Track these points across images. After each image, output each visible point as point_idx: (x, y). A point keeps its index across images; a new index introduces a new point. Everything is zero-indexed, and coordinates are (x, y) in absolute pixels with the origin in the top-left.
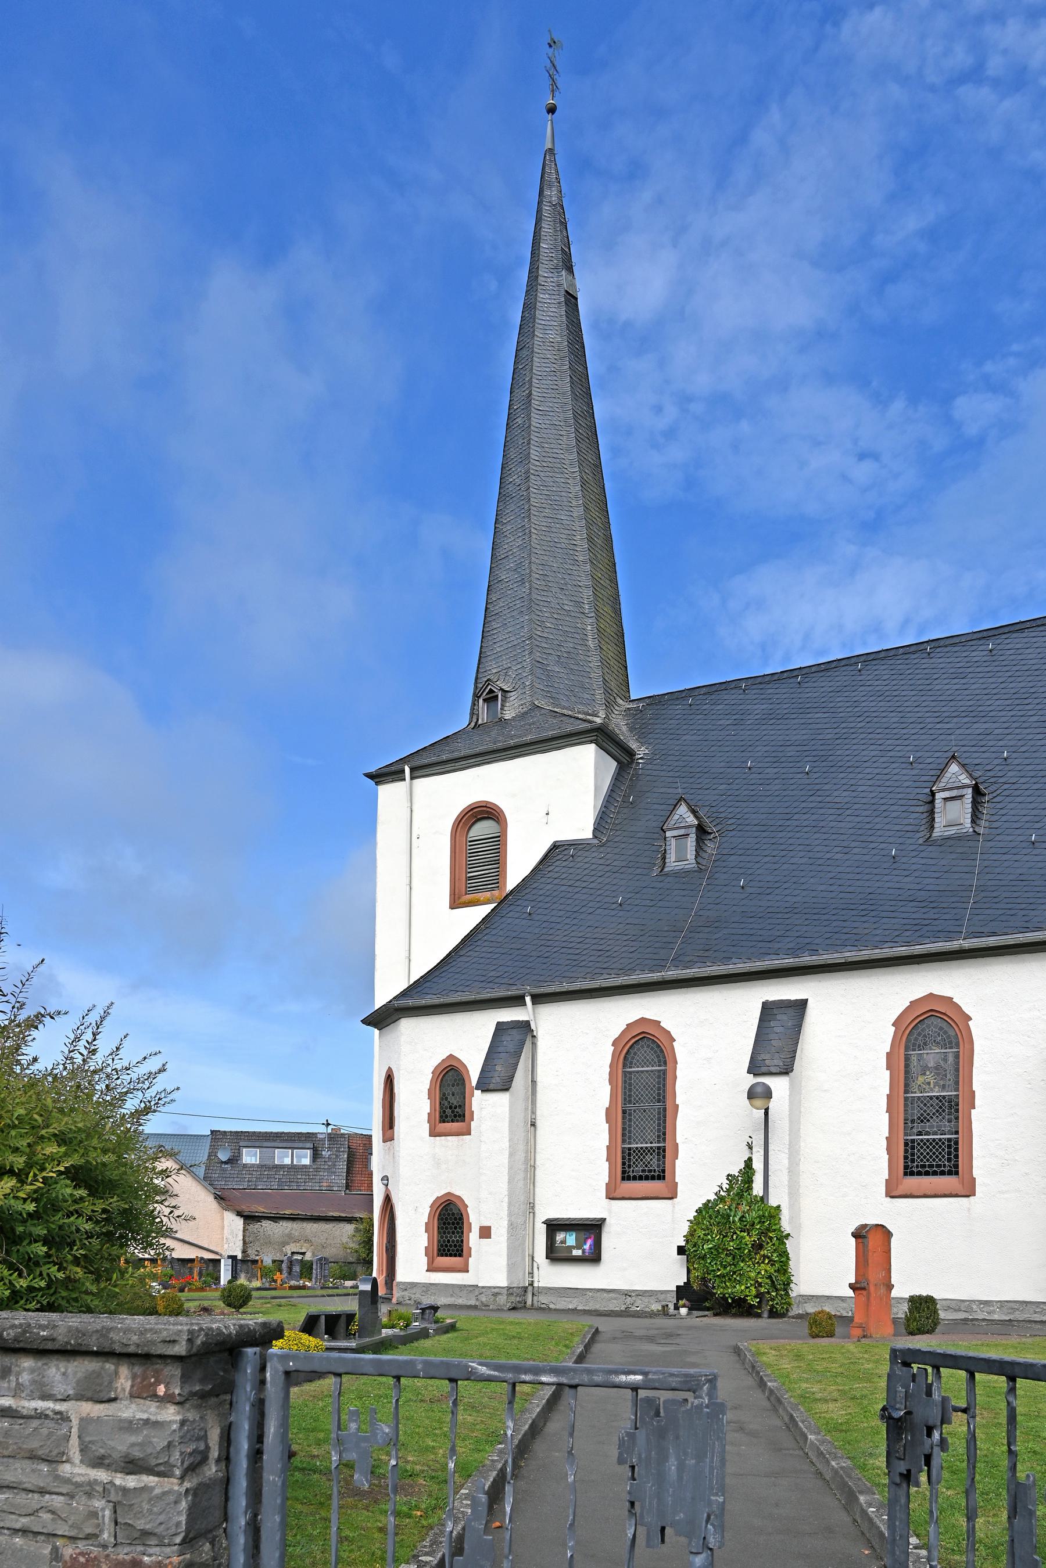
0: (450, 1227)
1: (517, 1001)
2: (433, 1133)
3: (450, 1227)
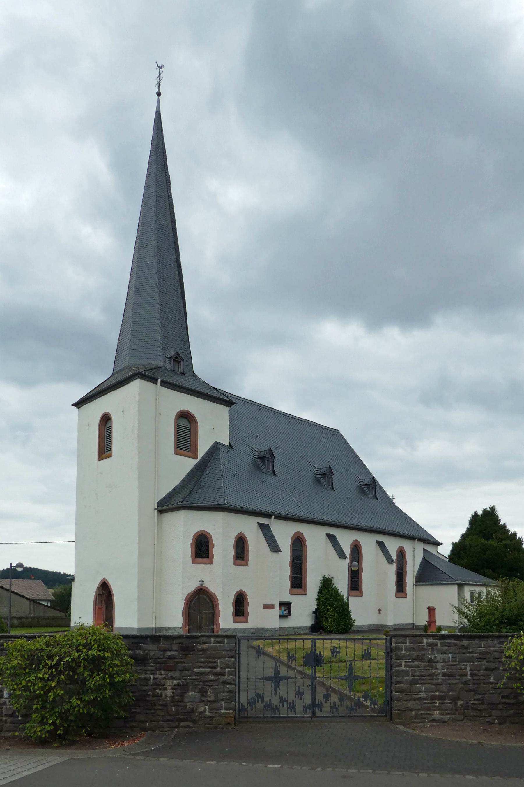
0: (240, 603)
1: (268, 515)
3: (240, 603)
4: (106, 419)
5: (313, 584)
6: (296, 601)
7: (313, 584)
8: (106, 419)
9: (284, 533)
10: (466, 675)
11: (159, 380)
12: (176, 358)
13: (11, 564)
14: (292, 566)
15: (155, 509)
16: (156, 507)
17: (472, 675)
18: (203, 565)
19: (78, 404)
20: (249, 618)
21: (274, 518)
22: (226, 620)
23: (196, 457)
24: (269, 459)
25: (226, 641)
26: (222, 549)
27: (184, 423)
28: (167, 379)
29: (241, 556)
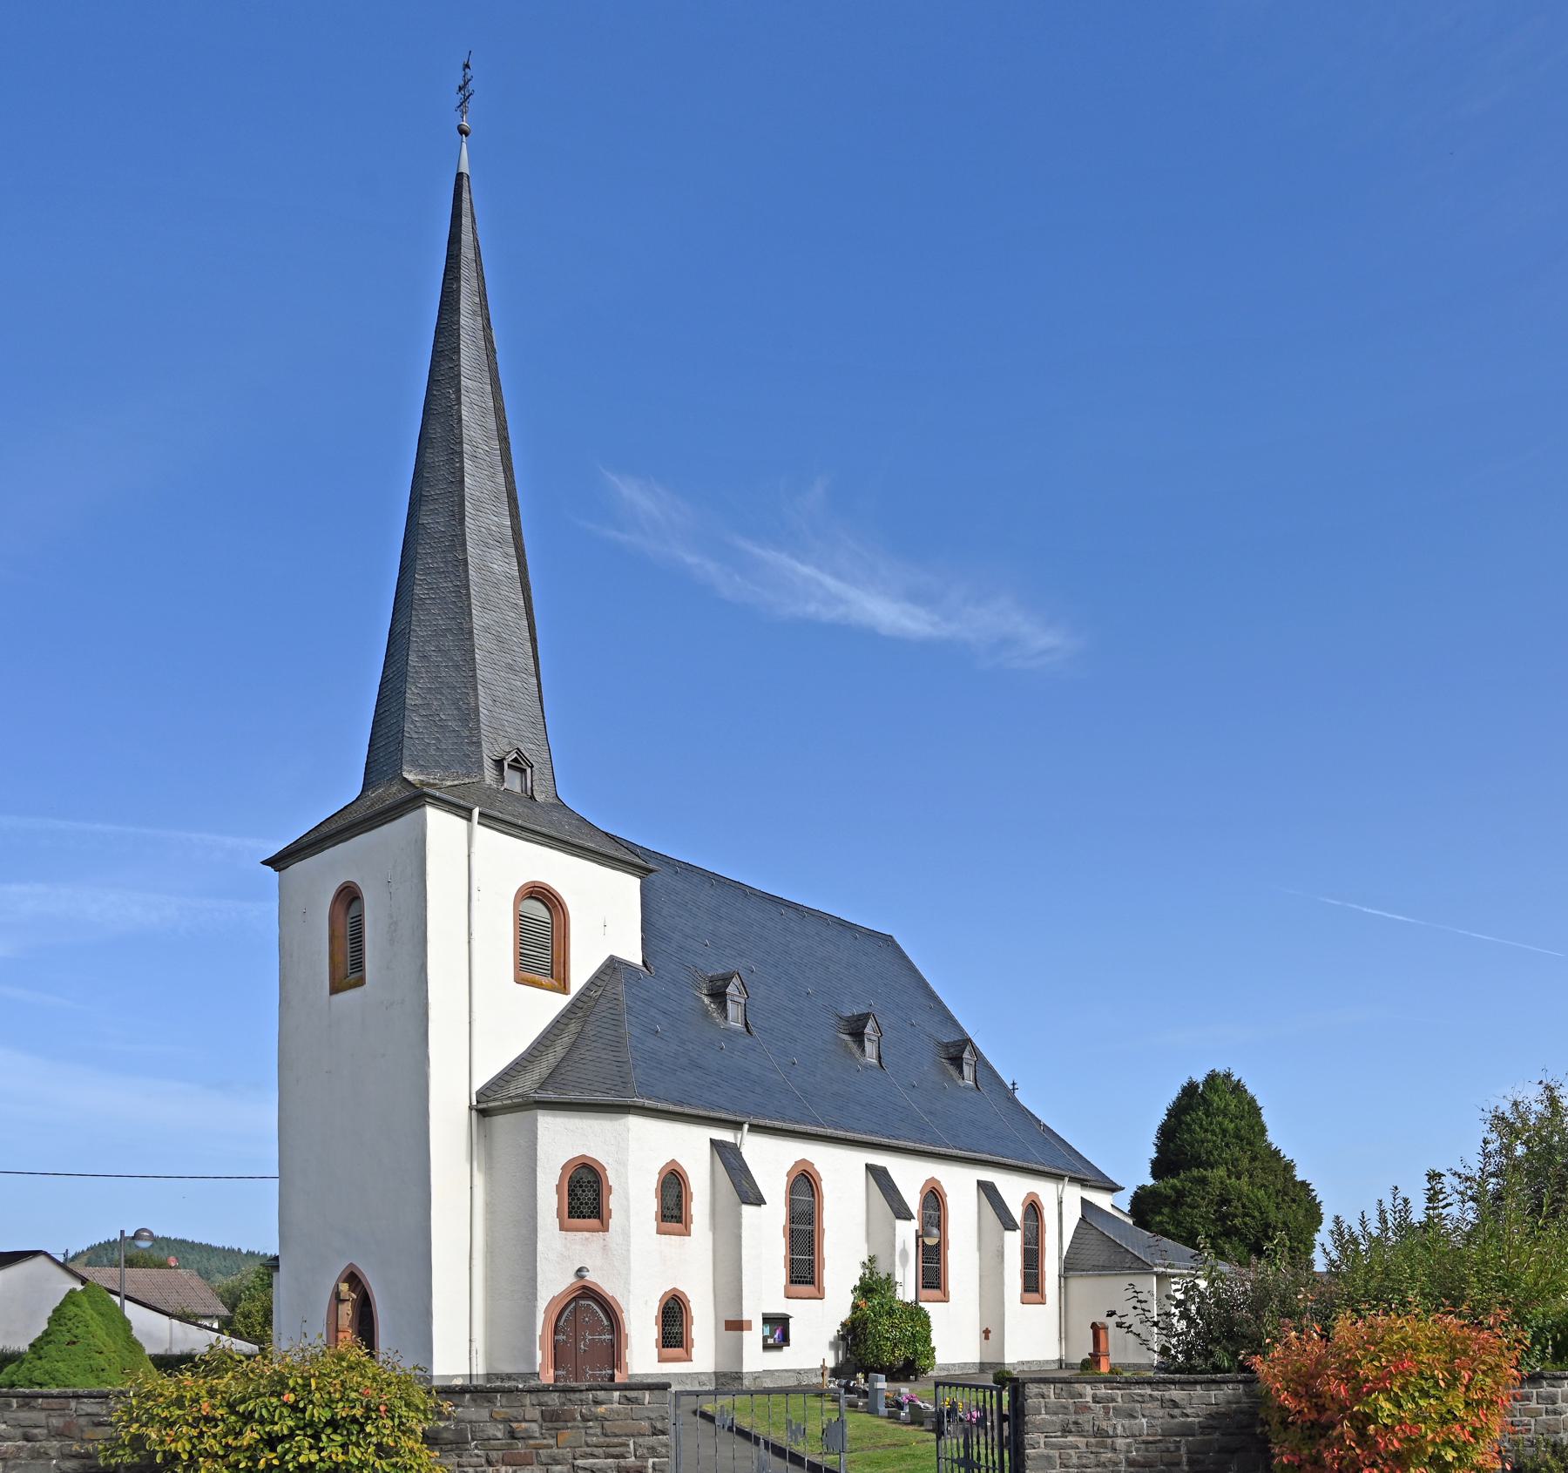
0: (673, 1315)
1: (736, 1126)
2: (659, 1232)
3: (673, 1315)
4: (349, 896)
5: (841, 1269)
6: (801, 1313)
7: (841, 1269)
8: (349, 896)
9: (772, 1161)
10: (1178, 1464)
11: (476, 811)
12: (515, 760)
13: (122, 1232)
14: (791, 1236)
15: (471, 1108)
17: (1190, 1462)
18: (587, 1234)
19: (278, 862)
20: (695, 1352)
22: (642, 1355)
23: (564, 989)
25: (647, 1395)
26: (633, 1198)
27: (538, 910)
28: (755, 1122)
29: (675, 1212)
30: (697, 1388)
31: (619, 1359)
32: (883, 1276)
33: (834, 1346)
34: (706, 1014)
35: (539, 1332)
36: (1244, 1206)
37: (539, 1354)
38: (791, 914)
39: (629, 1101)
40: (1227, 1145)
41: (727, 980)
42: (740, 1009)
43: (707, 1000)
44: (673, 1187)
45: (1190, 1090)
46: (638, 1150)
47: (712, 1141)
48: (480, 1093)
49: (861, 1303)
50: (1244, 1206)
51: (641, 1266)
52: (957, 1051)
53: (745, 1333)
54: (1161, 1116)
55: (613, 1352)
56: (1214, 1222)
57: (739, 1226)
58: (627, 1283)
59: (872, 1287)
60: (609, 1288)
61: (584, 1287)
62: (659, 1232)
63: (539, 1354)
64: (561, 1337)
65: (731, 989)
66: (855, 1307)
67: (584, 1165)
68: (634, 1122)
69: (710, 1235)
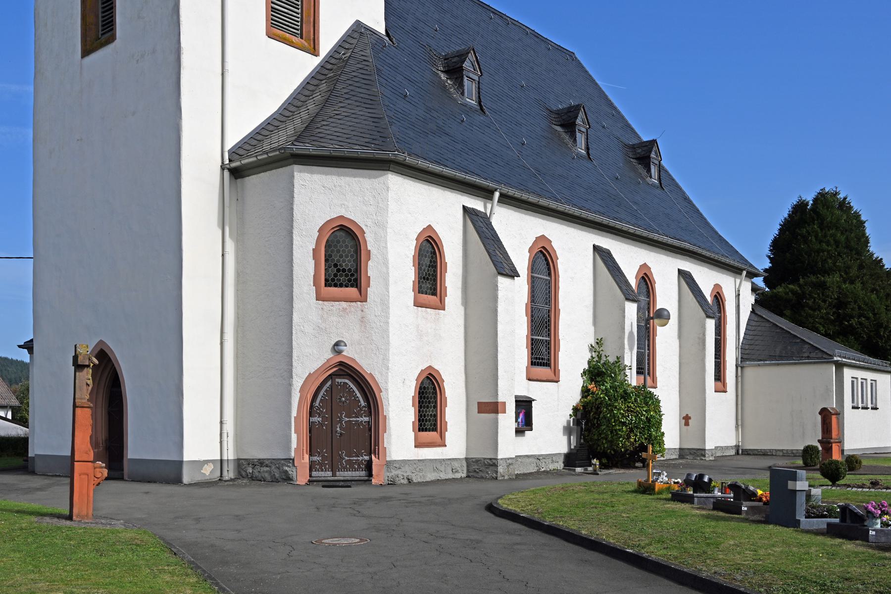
0: (429, 393)
1: (486, 193)
2: (417, 304)
3: (429, 393)
9: (517, 231)
15: (223, 168)
16: (227, 162)
18: (344, 304)
21: (746, 276)
22: (399, 439)
23: (315, 52)
24: (471, 75)
26: (392, 266)
28: (505, 190)
30: (450, 476)
31: (377, 443)
32: (612, 359)
33: (568, 431)
34: (444, 88)
35: (294, 413)
36: (860, 308)
37: (294, 437)
38: (498, 20)
39: (391, 155)
40: (839, 254)
41: (462, 56)
42: (474, 87)
43: (443, 76)
44: (429, 253)
45: (800, 208)
46: (404, 211)
47: (465, 208)
48: (232, 152)
49: (591, 386)
50: (860, 308)
51: (404, 341)
52: (643, 154)
53: (500, 416)
54: (774, 231)
55: (369, 436)
56: (832, 322)
57: (495, 299)
58: (386, 359)
59: (598, 372)
60: (366, 364)
61: (341, 364)
62: (417, 304)
63: (294, 437)
64: (317, 419)
65: (467, 65)
66: (585, 392)
67: (342, 228)
68: (394, 181)
69: (461, 310)
